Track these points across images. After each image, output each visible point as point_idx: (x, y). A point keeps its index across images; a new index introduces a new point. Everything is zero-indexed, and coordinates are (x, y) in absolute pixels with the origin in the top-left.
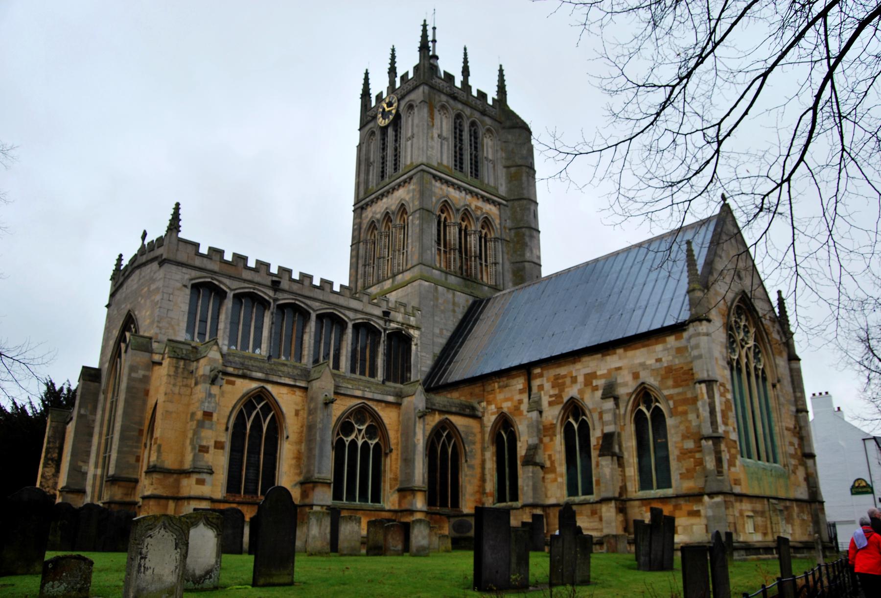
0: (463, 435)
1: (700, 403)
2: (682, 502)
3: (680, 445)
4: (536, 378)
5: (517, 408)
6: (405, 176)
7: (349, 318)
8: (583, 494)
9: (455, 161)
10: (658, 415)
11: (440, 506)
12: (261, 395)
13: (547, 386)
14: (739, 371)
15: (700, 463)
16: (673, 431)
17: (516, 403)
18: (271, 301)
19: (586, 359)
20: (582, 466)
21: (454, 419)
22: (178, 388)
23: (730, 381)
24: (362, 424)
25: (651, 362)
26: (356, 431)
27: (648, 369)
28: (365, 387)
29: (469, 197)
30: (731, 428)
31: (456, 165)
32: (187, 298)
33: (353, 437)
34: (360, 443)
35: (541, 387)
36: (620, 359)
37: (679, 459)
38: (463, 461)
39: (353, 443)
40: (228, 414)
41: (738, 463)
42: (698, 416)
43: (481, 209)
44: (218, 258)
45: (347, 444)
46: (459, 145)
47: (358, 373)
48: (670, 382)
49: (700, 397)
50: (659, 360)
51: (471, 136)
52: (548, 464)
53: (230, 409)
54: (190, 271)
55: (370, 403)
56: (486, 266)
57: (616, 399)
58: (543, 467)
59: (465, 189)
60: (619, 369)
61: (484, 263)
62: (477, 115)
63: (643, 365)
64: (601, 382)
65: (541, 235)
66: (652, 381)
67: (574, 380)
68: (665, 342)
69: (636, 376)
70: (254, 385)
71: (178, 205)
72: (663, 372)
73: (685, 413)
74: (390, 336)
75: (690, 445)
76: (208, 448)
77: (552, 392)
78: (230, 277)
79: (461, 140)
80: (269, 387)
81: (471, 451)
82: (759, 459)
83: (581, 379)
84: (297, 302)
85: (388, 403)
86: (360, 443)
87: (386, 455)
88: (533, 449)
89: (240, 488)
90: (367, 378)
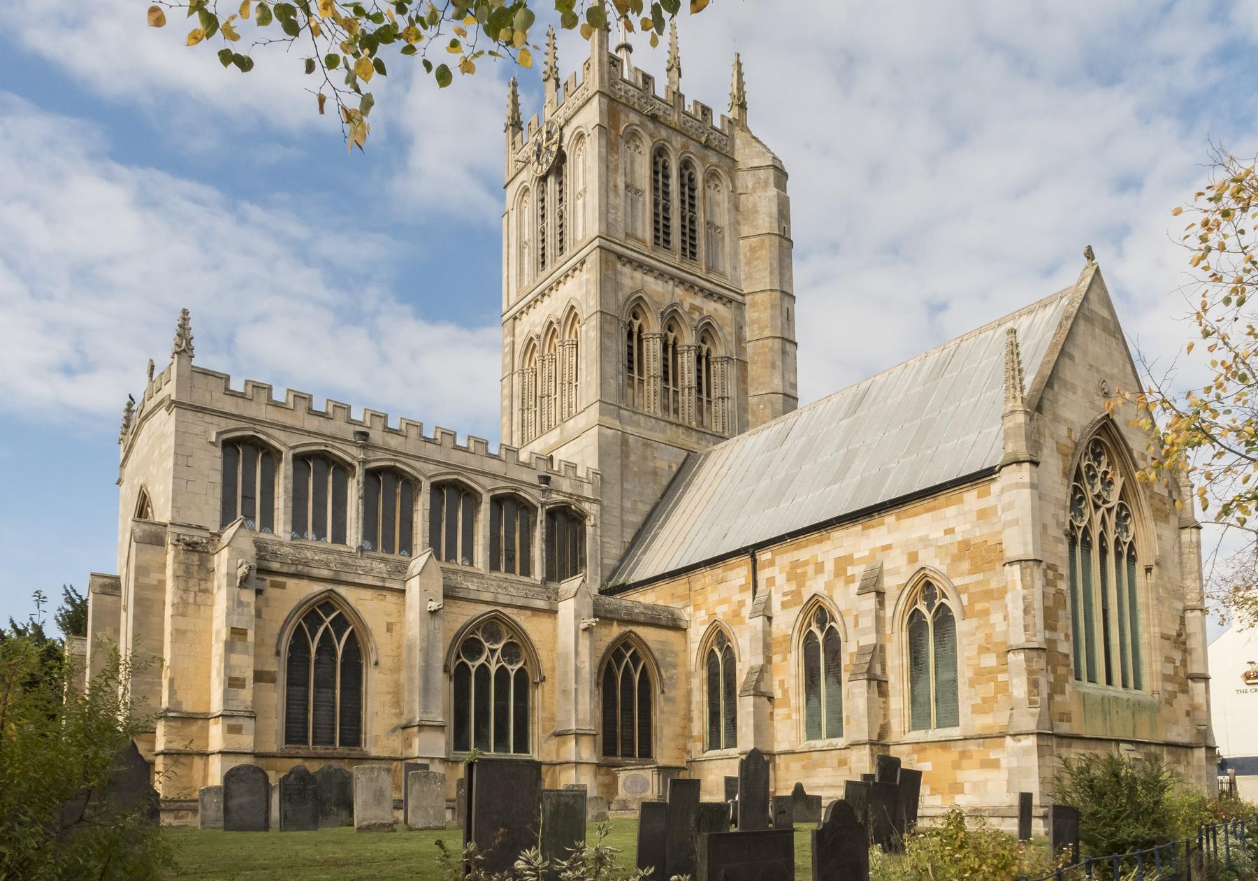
0: (657, 654)
1: (1009, 597)
2: (972, 746)
3: (975, 662)
4: (764, 567)
5: (736, 614)
6: (574, 260)
7: (483, 487)
8: (829, 737)
9: (657, 230)
10: (944, 619)
11: (622, 755)
12: (327, 603)
13: (781, 579)
14: (1087, 545)
15: (1004, 688)
16: (965, 641)
17: (735, 607)
18: (356, 463)
19: (838, 534)
20: (828, 696)
21: (642, 631)
22: (192, 595)
23: (1067, 562)
24: (497, 642)
25: (937, 534)
26: (487, 652)
27: (931, 546)
28: (499, 586)
29: (679, 291)
30: (1062, 636)
31: (657, 237)
32: (218, 464)
33: (482, 660)
34: (493, 669)
35: (771, 581)
36: (889, 532)
37: (972, 684)
38: (658, 692)
39: (483, 669)
40: (277, 631)
41: (1068, 688)
42: (1005, 618)
43: (700, 309)
44: (263, 396)
45: (473, 671)
46: (662, 202)
47: (503, 569)
48: (965, 565)
49: (1009, 587)
50: (949, 531)
51: (683, 185)
52: (778, 694)
53: (281, 624)
54: (216, 420)
55: (507, 611)
56: (709, 402)
57: (880, 594)
58: (771, 699)
59: (672, 278)
60: (887, 548)
61: (705, 399)
62: (693, 147)
63: (924, 540)
64: (858, 571)
65: (800, 353)
66: (934, 563)
67: (820, 568)
68: (961, 501)
69: (913, 558)
70: (318, 588)
71: (185, 312)
72: (955, 551)
73: (986, 613)
74: (551, 514)
75: (990, 661)
76: (244, 680)
77: (787, 588)
78: (285, 428)
79: (666, 193)
80: (342, 590)
81: (671, 678)
82: (1109, 681)
83: (829, 566)
84: (398, 465)
85: (535, 610)
86: (493, 669)
87: (537, 684)
88: (762, 672)
89: (306, 737)
90: (517, 577)
